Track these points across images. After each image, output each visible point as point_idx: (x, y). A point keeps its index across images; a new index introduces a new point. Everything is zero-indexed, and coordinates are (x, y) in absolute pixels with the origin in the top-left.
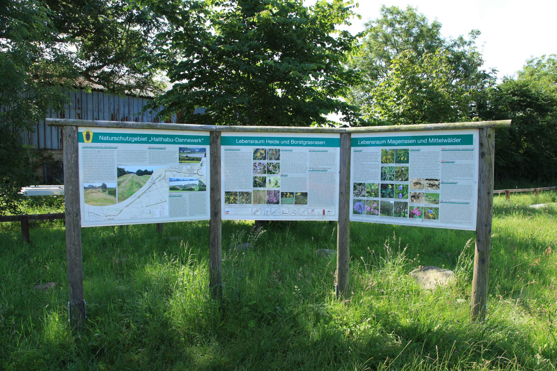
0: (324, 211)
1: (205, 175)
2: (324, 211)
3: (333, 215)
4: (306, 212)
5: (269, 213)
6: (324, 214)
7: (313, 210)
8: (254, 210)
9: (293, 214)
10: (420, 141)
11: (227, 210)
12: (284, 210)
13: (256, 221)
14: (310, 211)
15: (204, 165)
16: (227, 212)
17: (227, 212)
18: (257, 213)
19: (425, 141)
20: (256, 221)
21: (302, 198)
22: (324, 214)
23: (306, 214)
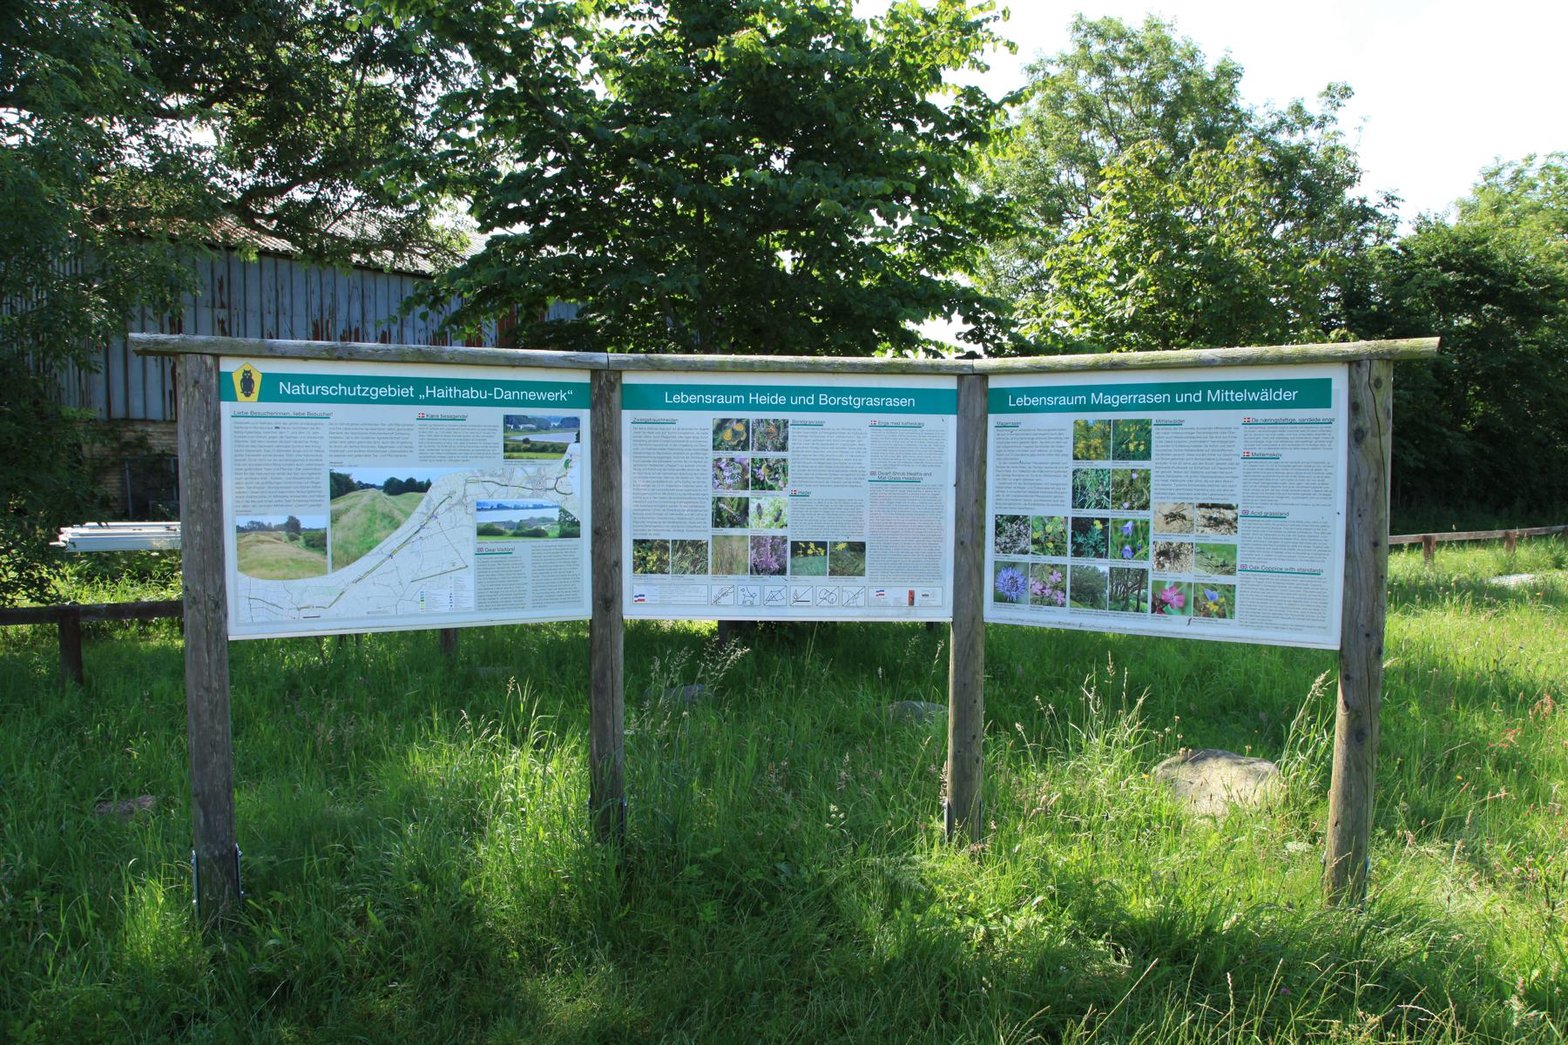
0: (912, 594)
1: (578, 494)
2: (912, 594)
3: (937, 606)
4: (862, 596)
5: (756, 601)
6: (912, 602)
7: (881, 593)
8: (716, 591)
9: (825, 603)
10: (1183, 398)
11: (639, 590)
12: (800, 591)
14: (873, 593)
15: (575, 464)
16: (640, 598)
17: (640, 598)
18: (723, 601)
19: (1196, 397)
22: (912, 602)
23: (860, 601)
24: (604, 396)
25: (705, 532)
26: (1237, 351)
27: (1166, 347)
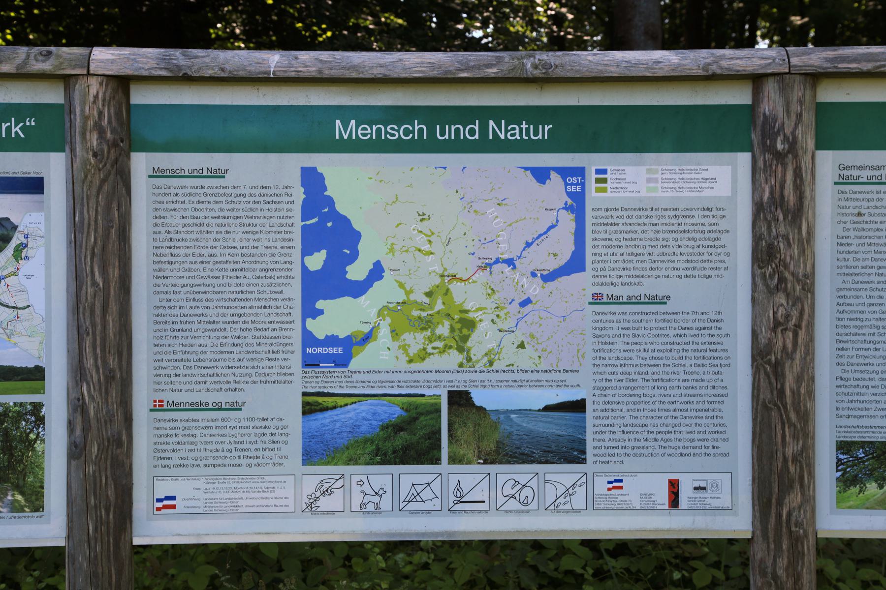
0: (674, 485)
1: (39, 304)
2: (674, 485)
3: (724, 510)
4: (580, 491)
5: (386, 503)
6: (674, 501)
7: (616, 484)
8: (310, 485)
9: (513, 504)
10: (449, 132)
11: (163, 489)
12: (467, 482)
13: (544, 183)
14: (601, 485)
15: (36, 252)
16: (167, 503)
17: (167, 503)
18: (324, 503)
19: (471, 131)
20: (544, 183)
21: (557, 437)
22: (674, 501)
23: (579, 500)
24: (124, 132)
25: (458, 369)
26: (307, 60)
27: (614, 43)
